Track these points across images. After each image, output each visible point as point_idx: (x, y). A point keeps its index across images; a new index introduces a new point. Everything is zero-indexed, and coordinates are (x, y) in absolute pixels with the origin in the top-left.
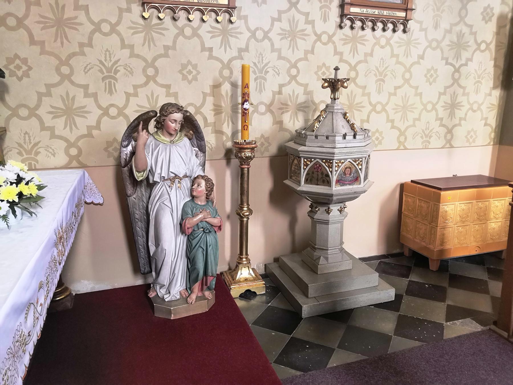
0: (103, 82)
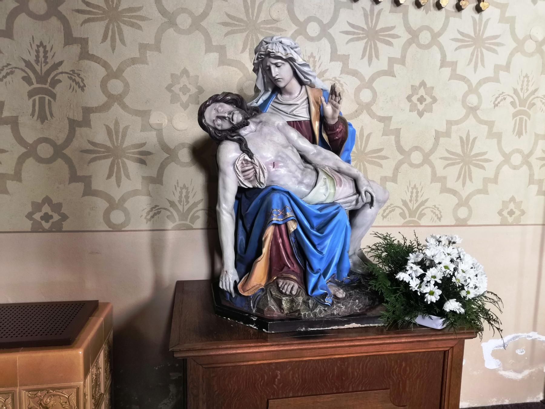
0: (513, 119)
